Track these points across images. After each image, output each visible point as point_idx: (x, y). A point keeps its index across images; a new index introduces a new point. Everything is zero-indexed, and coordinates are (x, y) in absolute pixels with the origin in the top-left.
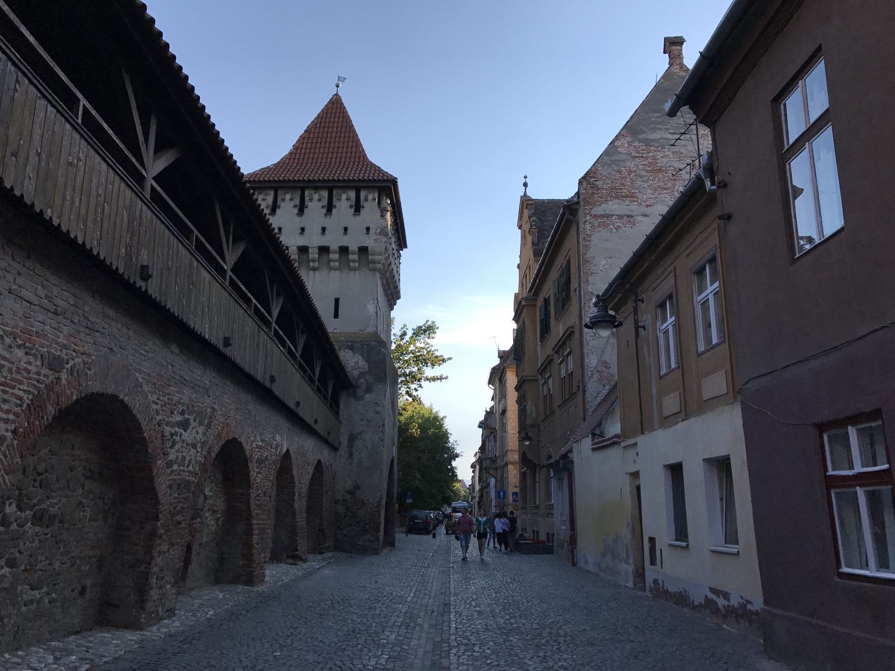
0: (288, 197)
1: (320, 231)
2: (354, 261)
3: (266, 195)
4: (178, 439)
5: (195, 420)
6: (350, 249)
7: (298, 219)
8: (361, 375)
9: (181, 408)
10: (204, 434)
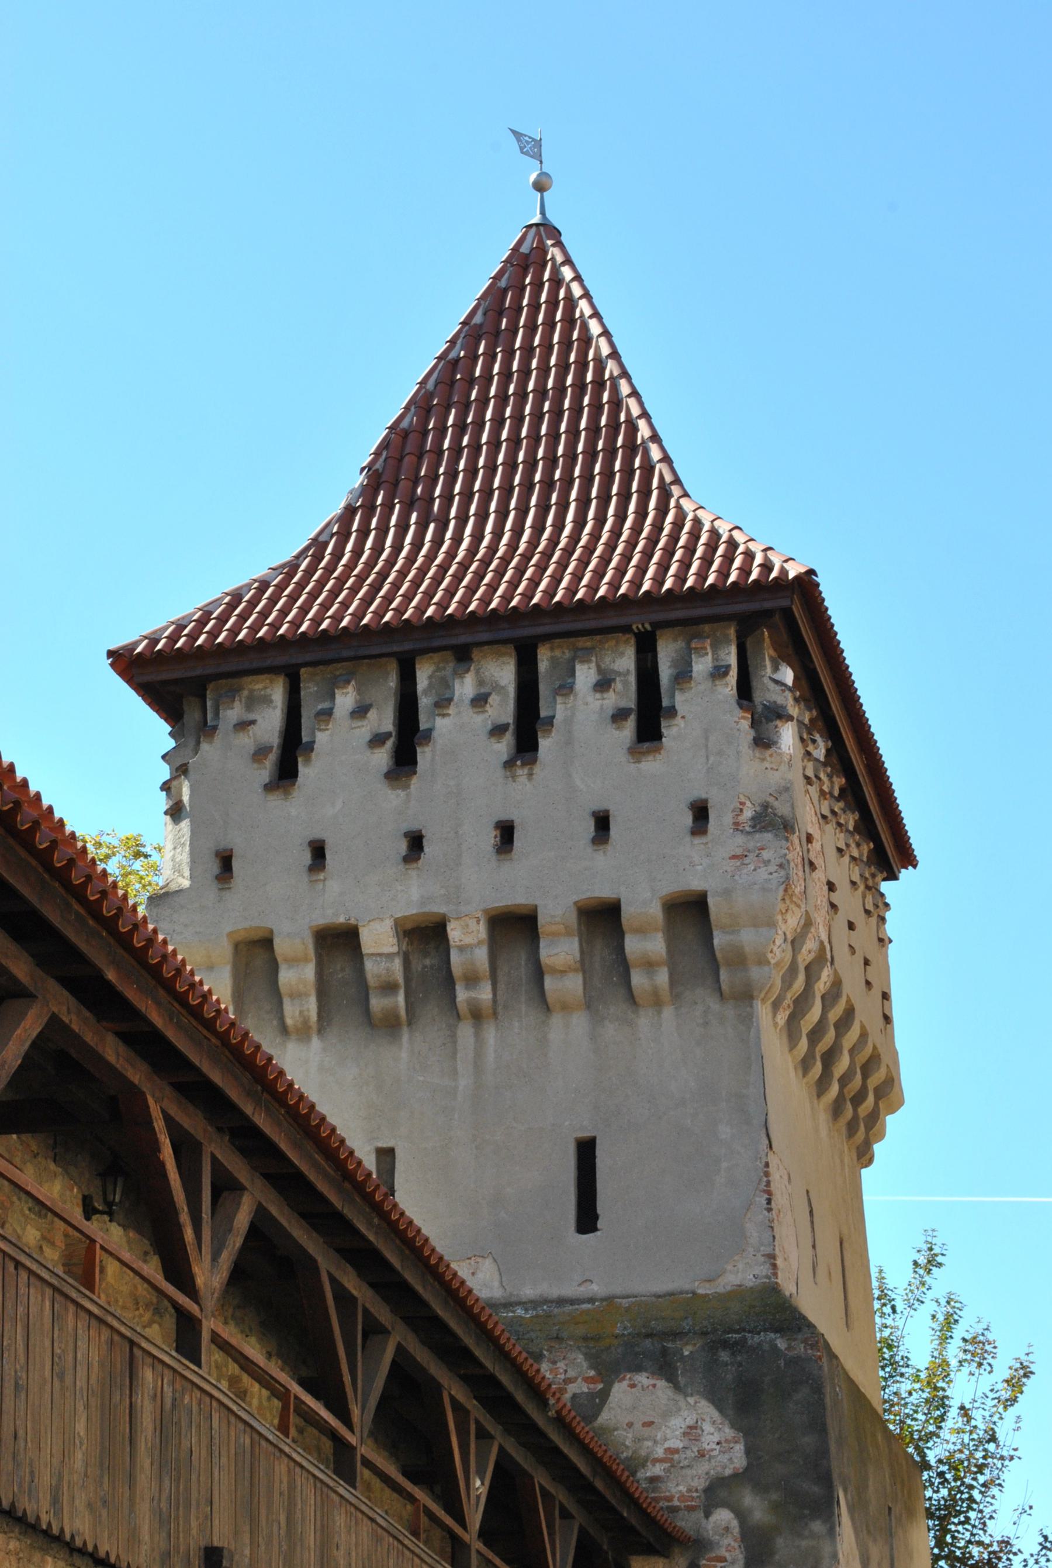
0: (345, 700)
1: (490, 838)
3: (251, 703)
6: (627, 912)
7: (392, 798)
8: (717, 1491)
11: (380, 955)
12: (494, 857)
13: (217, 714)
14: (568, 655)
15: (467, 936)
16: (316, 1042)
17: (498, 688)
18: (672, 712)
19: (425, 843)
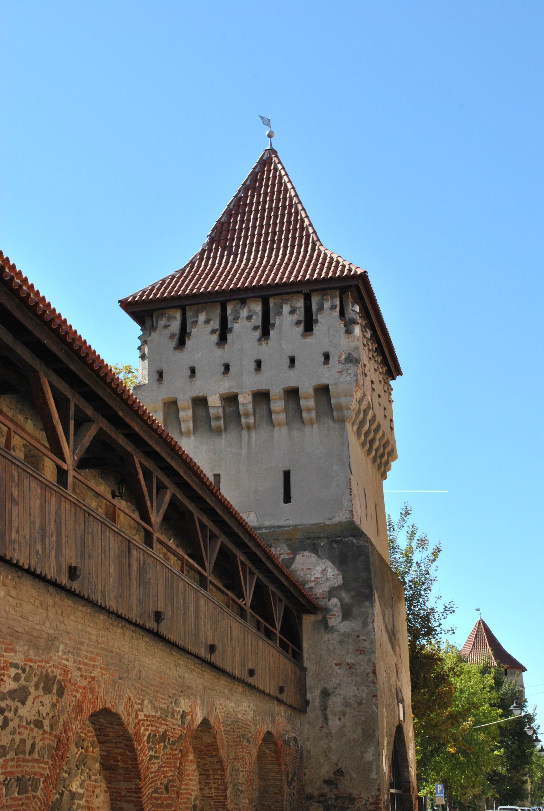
1: (253, 365)
2: (309, 410)
3: (169, 318)
4: (10, 715)
5: (37, 687)
7: (219, 352)
8: (332, 592)
9: (13, 672)
10: (54, 705)
11: (215, 407)
16: (192, 438)
17: (256, 313)
18: (317, 321)
19: (230, 368)
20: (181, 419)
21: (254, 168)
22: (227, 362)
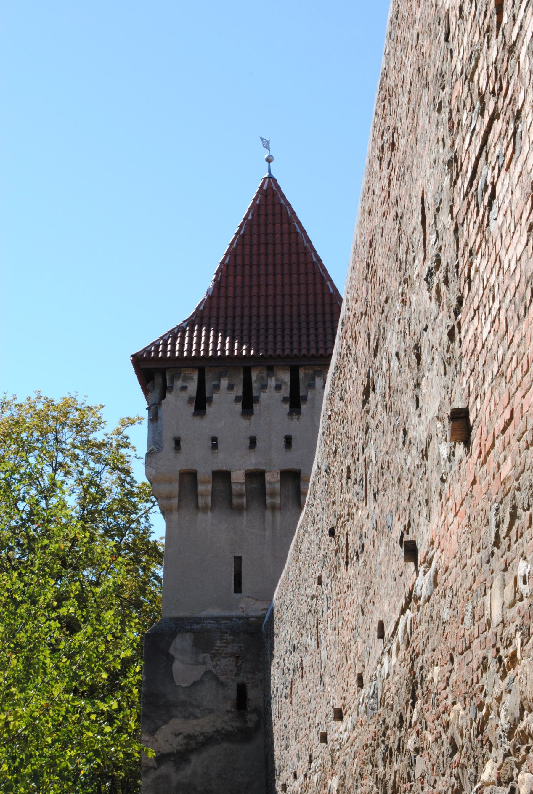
0: (224, 383)
1: (282, 442)
3: (185, 379)
7: (244, 423)
11: (238, 483)
12: (284, 450)
13: (172, 382)
14: (311, 372)
15: (272, 479)
16: (210, 514)
17: (284, 382)
19: (257, 441)
20: (199, 493)
21: (255, 200)
22: (253, 435)
